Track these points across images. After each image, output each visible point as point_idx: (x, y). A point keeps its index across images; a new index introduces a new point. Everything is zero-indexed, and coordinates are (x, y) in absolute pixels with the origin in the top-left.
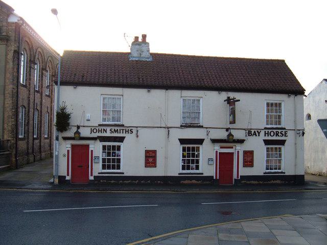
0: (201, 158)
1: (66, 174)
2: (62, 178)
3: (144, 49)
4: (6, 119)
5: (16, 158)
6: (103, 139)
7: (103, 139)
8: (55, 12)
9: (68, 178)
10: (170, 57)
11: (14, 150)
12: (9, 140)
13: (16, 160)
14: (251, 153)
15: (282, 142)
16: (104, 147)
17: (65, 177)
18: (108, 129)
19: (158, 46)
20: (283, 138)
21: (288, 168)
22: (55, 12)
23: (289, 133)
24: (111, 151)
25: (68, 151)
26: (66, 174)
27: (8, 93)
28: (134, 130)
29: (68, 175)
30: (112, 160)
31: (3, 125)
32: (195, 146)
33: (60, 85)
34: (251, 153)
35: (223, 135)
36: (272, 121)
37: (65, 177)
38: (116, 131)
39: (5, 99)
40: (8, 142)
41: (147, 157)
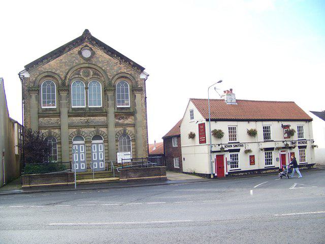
0: (273, 158)
3: (233, 97)
6: (230, 151)
7: (230, 151)
8: (220, 82)
14: (254, 156)
15: (305, 147)
16: (231, 155)
18: (233, 145)
19: (240, 95)
20: (305, 145)
21: (308, 161)
22: (220, 82)
23: (308, 142)
28: (244, 144)
30: (234, 164)
32: (270, 151)
34: (254, 156)
35: (282, 145)
38: (236, 146)
41: (254, 162)
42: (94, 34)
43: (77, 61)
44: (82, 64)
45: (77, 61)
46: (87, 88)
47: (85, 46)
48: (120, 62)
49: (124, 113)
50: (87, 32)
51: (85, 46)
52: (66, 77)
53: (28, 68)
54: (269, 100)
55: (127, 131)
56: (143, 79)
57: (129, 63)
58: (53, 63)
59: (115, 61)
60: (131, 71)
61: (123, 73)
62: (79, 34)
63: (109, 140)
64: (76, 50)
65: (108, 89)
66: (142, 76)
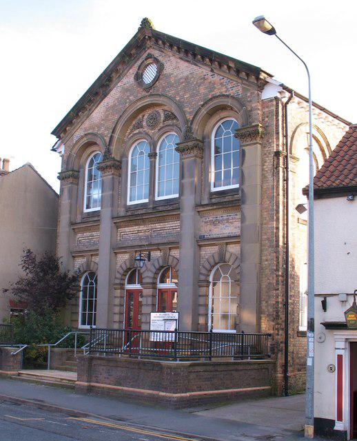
1: (334, 417)
2: (323, 426)
4: (264, 292)
5: (285, 371)
9: (339, 426)
10: (97, 84)
11: (281, 356)
12: (270, 335)
13: (286, 378)
17: (332, 423)
24: (87, 312)
25: (340, 358)
26: (334, 417)
27: (268, 239)
29: (340, 418)
31: (260, 303)
33: (315, 199)
36: (227, 173)
37: (332, 423)
39: (261, 251)
40: (267, 339)
42: (158, 26)
43: (131, 98)
44: (135, 102)
45: (131, 98)
46: (153, 155)
47: (147, 59)
48: (212, 71)
49: (230, 202)
50: (145, 23)
51: (147, 59)
52: (111, 138)
53: (61, 131)
54: (36, 169)
55: (228, 256)
56: (271, 100)
57: (229, 68)
58: (98, 113)
59: (202, 71)
60: (233, 87)
61: (211, 99)
62: (129, 31)
63: (180, 275)
64: (128, 79)
65: (193, 146)
66: (269, 93)
